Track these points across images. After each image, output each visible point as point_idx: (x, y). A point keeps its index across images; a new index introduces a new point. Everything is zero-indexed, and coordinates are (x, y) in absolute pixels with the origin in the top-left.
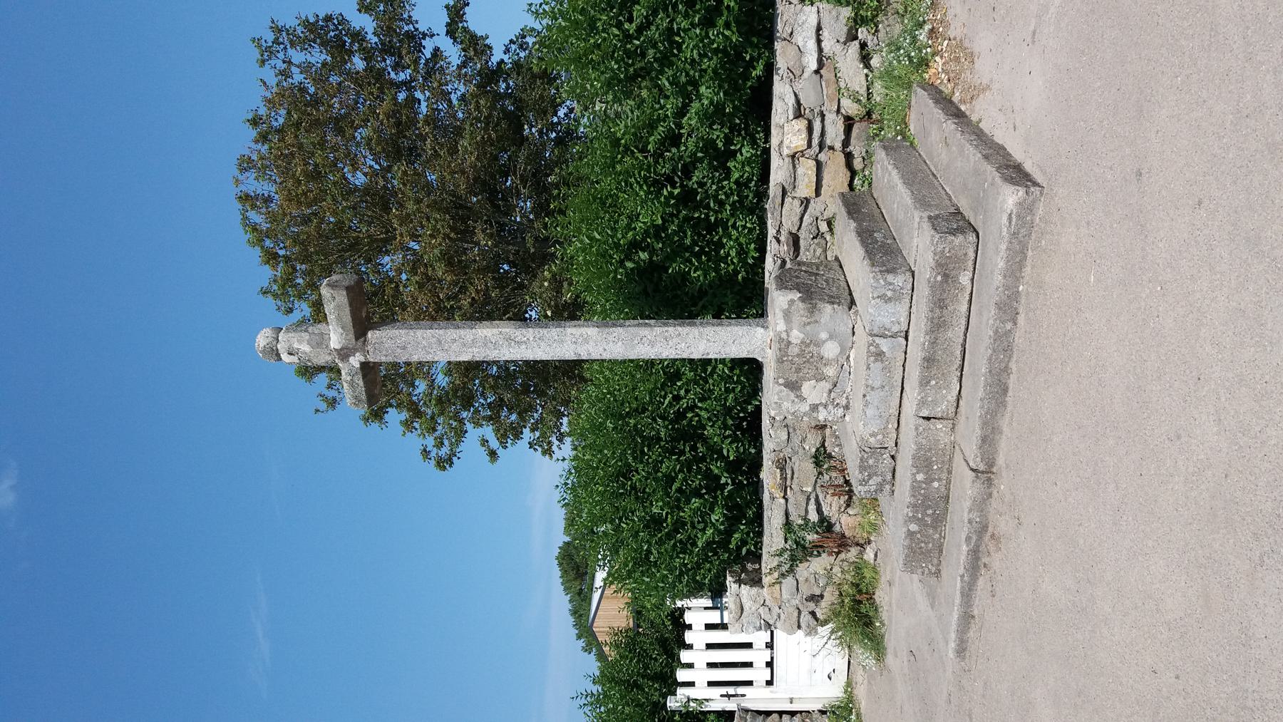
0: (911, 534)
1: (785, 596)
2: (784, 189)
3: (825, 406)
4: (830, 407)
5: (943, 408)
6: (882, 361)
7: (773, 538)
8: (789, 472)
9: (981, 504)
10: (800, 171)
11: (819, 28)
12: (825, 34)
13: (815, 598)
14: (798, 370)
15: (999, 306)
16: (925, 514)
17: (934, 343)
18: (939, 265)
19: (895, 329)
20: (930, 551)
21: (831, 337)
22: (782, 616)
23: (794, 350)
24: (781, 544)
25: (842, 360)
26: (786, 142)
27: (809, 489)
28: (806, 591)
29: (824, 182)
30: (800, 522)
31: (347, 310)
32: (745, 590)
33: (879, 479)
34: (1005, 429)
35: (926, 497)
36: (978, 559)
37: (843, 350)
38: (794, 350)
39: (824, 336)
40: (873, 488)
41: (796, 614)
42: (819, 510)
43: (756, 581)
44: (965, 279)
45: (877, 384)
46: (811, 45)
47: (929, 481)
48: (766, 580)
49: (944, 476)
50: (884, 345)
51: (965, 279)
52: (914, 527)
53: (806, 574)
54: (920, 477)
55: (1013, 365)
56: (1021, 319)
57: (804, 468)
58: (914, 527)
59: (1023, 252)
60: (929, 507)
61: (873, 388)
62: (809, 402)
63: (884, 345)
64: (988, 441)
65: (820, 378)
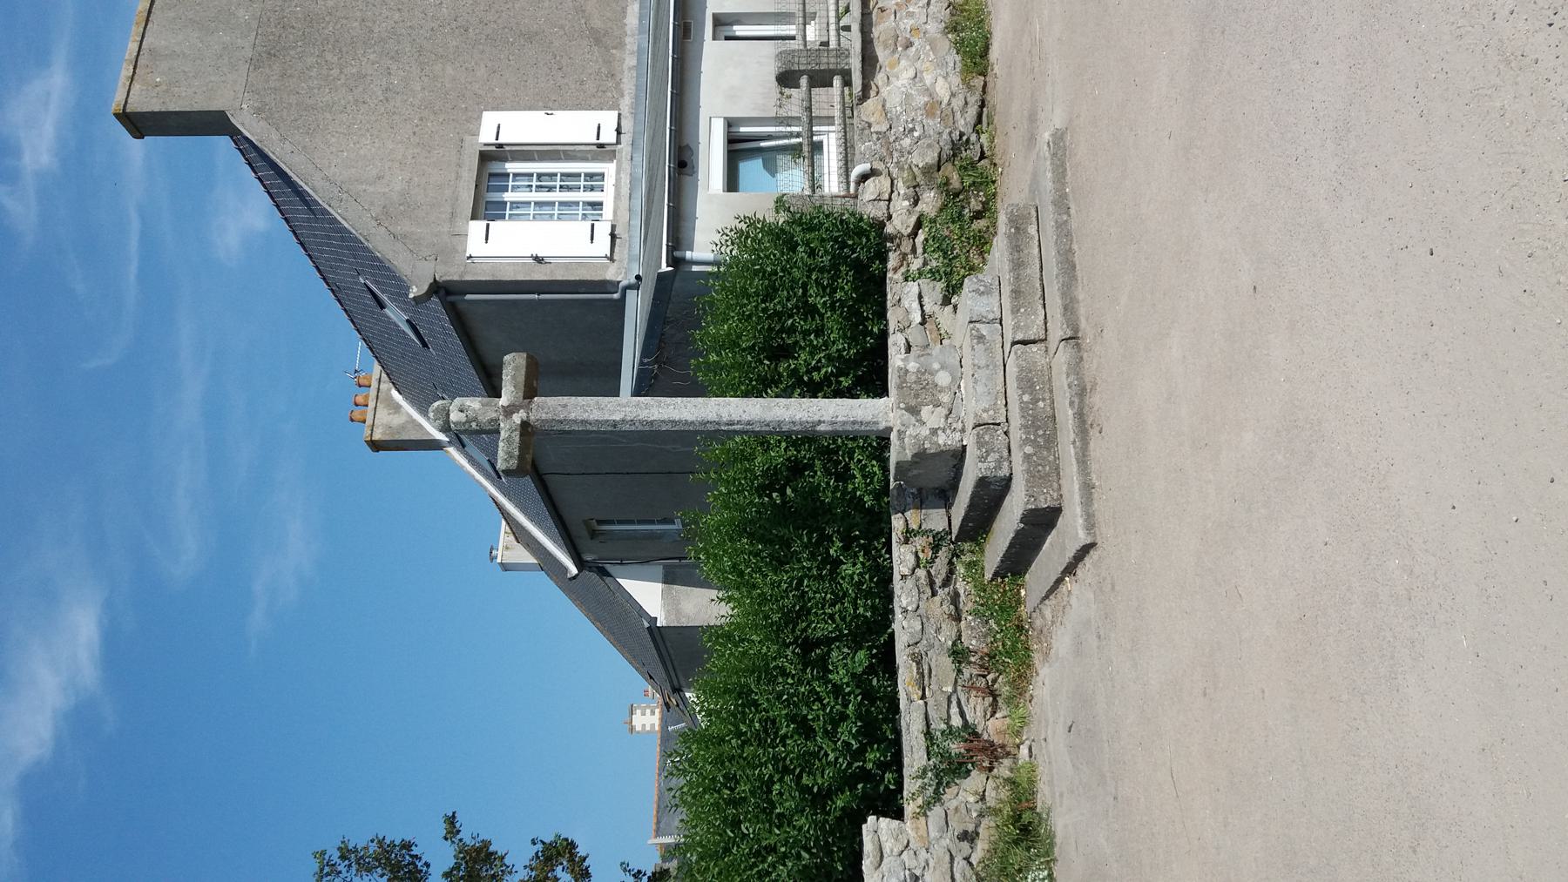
1: (934, 834)
5: (1034, 331)
7: (915, 757)
8: (926, 667)
9: (1076, 367)
11: (920, 297)
12: (926, 300)
13: (968, 837)
14: (917, 396)
15: (1054, 203)
16: (1036, 436)
17: (1017, 278)
18: (1010, 221)
19: (991, 316)
20: (1048, 475)
21: (942, 368)
22: (932, 864)
23: (912, 378)
24: (924, 762)
25: (955, 389)
27: (950, 689)
28: (957, 827)
30: (943, 726)
31: (523, 372)
32: (884, 822)
33: (997, 456)
34: (1081, 297)
35: (1035, 418)
36: (1084, 422)
37: (953, 379)
38: (912, 378)
39: (936, 366)
40: (992, 465)
41: (947, 858)
42: (962, 714)
43: (899, 815)
44: (1032, 230)
45: (983, 363)
46: (916, 305)
47: (1035, 401)
48: (910, 808)
49: (1047, 395)
50: (984, 329)
51: (1032, 230)
52: (1029, 450)
53: (954, 803)
54: (1026, 398)
55: (1075, 247)
56: (1072, 211)
57: (942, 664)
59: (1063, 165)
60: (1039, 428)
62: (929, 425)
63: (984, 329)
64: (1069, 309)
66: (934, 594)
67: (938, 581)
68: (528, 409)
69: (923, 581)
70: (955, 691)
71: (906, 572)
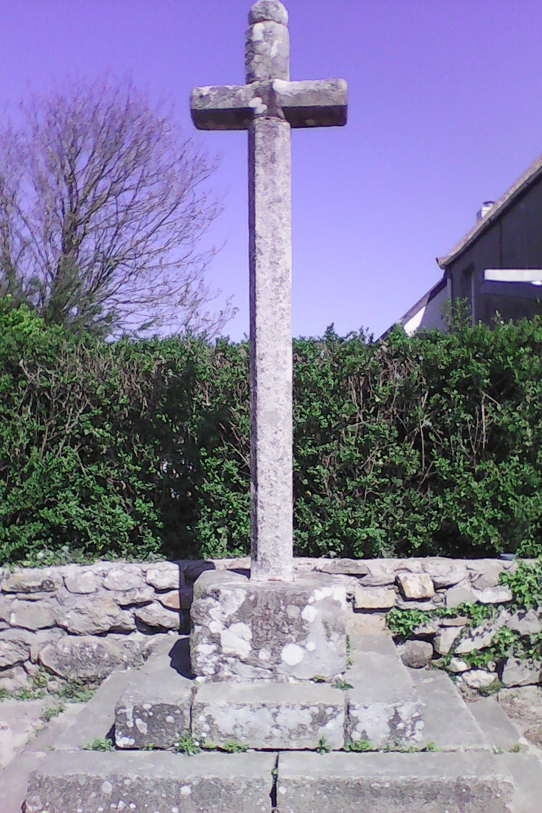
0: (97, 785)
2: (364, 575)
3: (218, 652)
4: (215, 658)
6: (312, 724)
10: (382, 591)
23: (293, 611)
26: (409, 575)
27: (13, 621)
29: (367, 616)
33: (144, 730)
39: (311, 646)
52: (108, 788)
58: (108, 788)
61: (275, 715)
65: (256, 644)
66: (123, 607)
67: (139, 612)
68: (269, 114)
69: (140, 596)
70: (12, 627)
71: (150, 577)
